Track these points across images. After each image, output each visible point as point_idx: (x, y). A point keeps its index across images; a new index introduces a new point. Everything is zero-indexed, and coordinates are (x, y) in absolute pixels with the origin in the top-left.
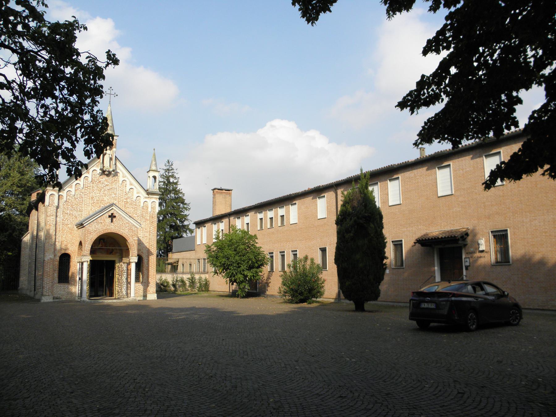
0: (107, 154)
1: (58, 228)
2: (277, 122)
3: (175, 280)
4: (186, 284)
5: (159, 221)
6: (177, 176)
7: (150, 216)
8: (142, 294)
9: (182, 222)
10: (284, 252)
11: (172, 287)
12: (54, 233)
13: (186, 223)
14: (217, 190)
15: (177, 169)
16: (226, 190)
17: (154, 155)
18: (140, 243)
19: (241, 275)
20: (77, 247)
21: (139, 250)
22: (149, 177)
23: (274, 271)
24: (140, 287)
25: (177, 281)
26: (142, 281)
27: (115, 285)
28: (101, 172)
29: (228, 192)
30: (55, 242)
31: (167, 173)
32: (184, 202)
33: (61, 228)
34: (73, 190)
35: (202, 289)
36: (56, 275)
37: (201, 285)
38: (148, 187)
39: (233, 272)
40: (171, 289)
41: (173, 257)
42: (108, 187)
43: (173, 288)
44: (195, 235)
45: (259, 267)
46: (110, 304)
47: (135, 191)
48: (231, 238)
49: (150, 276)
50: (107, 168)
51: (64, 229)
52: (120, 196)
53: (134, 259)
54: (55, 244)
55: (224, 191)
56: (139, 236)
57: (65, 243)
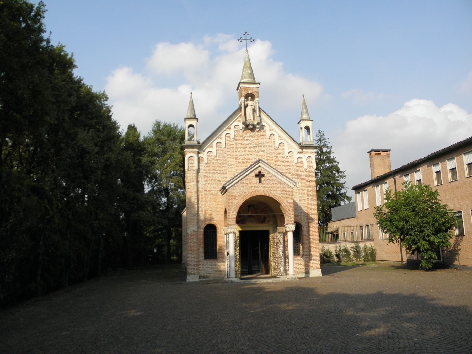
0: (249, 106)
1: (200, 195)
2: (413, 103)
3: (338, 250)
4: (350, 253)
5: (317, 191)
6: (329, 145)
7: (306, 175)
8: (304, 270)
9: (339, 191)
10: (460, 212)
11: (335, 257)
12: (196, 201)
13: (343, 191)
14: (373, 152)
15: (328, 138)
16: (383, 151)
17: (304, 102)
18: (297, 208)
19: (426, 242)
20: (223, 216)
21: (296, 216)
22: (301, 128)
23: (465, 234)
24: (300, 261)
25: (340, 251)
26: (303, 254)
27: (271, 260)
28: (244, 126)
29: (385, 153)
30: (198, 211)
31: (319, 144)
32: (339, 170)
33: (203, 195)
34: (214, 150)
35: (368, 259)
36: (201, 250)
37: (366, 254)
38: (301, 141)
39: (415, 238)
40: (334, 260)
41: (332, 226)
42: (254, 144)
43: (336, 259)
44: (354, 201)
45: (446, 231)
46: (263, 286)
47: (286, 146)
48: (406, 196)
49: (312, 248)
50: (251, 121)
51: (207, 196)
52: (268, 153)
53: (290, 227)
54: (198, 214)
55: (381, 152)
56: (295, 199)
57: (209, 212)
